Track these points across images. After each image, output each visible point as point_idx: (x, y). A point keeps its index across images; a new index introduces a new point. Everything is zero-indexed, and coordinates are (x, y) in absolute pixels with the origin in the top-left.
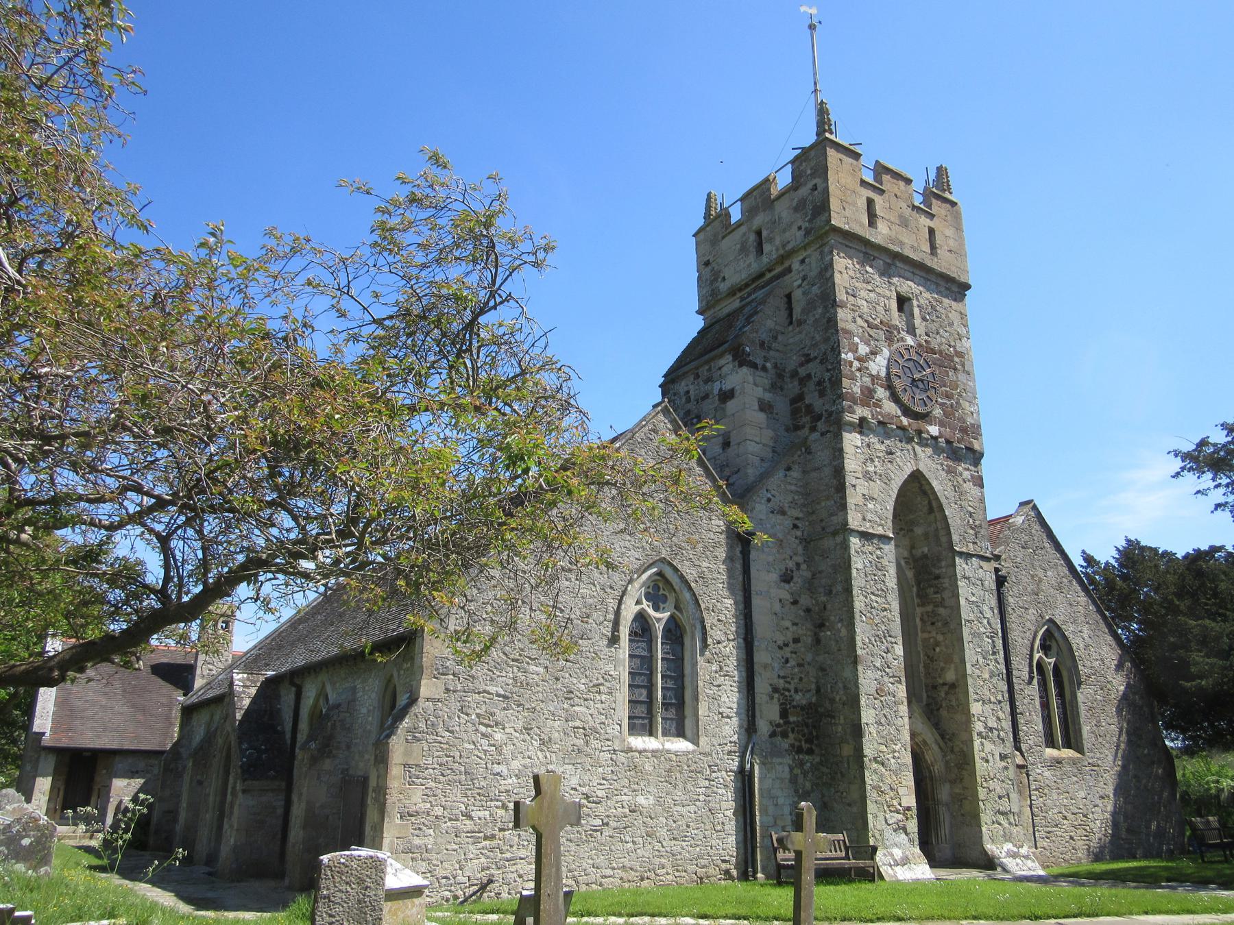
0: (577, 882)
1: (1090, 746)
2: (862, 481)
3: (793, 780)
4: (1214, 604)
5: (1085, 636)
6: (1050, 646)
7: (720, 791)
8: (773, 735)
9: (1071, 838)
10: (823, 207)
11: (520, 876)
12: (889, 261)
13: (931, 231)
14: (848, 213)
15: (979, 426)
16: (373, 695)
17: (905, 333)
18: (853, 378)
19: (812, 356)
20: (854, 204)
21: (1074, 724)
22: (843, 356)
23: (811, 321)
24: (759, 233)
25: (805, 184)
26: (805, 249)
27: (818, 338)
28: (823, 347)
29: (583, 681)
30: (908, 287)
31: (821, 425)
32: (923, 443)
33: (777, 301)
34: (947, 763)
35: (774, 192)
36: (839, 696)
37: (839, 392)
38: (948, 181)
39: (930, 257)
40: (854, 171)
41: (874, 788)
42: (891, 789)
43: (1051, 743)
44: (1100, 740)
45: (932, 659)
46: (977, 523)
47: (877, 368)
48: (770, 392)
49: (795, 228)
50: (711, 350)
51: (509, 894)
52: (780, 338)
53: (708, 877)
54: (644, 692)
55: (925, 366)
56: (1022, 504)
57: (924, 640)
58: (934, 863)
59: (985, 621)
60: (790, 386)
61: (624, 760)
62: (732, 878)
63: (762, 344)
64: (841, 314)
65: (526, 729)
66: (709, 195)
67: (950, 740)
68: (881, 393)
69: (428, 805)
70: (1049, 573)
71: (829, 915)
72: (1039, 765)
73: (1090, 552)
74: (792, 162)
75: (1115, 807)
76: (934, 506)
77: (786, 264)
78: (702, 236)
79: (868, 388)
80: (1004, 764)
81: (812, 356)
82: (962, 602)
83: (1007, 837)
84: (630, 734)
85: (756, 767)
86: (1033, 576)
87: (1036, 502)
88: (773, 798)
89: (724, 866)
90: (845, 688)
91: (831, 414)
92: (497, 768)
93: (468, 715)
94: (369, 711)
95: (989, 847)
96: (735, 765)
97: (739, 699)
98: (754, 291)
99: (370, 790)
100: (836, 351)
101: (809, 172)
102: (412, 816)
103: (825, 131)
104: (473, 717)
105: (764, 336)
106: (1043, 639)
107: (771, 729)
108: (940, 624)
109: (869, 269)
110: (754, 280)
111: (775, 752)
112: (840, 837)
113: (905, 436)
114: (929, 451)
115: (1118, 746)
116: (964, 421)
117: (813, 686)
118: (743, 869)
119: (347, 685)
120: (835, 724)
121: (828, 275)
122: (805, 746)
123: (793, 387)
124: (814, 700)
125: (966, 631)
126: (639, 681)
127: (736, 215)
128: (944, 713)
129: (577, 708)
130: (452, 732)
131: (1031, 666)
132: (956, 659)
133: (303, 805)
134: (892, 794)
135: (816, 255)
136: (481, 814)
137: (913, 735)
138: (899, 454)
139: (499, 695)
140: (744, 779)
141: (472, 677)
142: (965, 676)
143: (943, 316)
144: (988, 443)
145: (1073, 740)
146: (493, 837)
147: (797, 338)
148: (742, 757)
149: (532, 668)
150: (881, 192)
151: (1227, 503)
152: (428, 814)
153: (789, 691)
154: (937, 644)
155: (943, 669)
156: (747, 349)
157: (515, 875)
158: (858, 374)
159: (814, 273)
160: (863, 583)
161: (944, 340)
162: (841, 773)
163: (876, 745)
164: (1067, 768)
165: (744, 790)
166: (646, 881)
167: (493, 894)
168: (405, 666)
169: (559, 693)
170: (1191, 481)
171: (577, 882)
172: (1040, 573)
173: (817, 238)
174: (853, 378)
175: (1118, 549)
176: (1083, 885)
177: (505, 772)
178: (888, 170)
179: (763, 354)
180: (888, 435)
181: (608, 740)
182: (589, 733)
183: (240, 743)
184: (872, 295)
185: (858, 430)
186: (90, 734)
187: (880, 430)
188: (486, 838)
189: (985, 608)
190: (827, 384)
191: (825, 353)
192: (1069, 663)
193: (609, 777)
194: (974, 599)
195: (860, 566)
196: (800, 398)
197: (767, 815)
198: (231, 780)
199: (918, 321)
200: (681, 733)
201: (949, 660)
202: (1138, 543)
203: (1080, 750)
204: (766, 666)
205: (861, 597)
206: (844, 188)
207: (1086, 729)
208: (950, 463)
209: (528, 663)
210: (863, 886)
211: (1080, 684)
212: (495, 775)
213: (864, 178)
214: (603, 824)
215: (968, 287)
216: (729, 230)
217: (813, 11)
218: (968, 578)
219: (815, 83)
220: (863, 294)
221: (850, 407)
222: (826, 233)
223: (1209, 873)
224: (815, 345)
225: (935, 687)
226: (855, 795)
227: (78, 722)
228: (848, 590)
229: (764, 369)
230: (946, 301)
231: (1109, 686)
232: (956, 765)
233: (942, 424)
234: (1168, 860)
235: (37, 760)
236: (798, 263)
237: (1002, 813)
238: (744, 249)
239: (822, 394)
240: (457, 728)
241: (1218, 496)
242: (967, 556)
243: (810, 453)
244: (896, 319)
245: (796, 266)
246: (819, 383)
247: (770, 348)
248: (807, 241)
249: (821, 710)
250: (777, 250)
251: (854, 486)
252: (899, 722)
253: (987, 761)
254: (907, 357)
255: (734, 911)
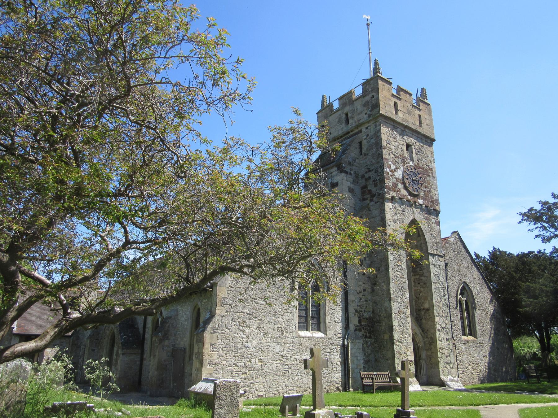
0: (279, 392)
1: (479, 335)
2: (393, 223)
3: (364, 349)
4: (531, 276)
5: (478, 289)
6: (464, 293)
7: (335, 354)
8: (355, 330)
9: (472, 373)
10: (376, 105)
11: (257, 390)
12: (403, 129)
13: (420, 116)
14: (387, 108)
15: (438, 200)
16: (188, 313)
17: (409, 160)
18: (389, 179)
19: (371, 169)
20: (389, 104)
21: (473, 326)
22: (385, 170)
23: (370, 154)
24: (347, 115)
25: (368, 95)
26: (368, 123)
27: (374, 161)
28: (376, 166)
29: (280, 307)
30: (410, 140)
31: (375, 199)
32: (416, 207)
33: (355, 145)
34: (424, 342)
35: (354, 97)
36: (383, 314)
37: (383, 185)
38: (426, 95)
39: (419, 127)
40: (389, 90)
41: (398, 352)
42: (404, 353)
43: (464, 334)
44: (484, 332)
45: (418, 298)
46: (438, 241)
47: (399, 175)
48: (353, 184)
49: (363, 114)
50: (327, 165)
51: (252, 397)
52: (357, 160)
53: (330, 390)
54: (304, 312)
55: (417, 174)
56: (453, 233)
57: (415, 290)
58: (421, 384)
59: (441, 283)
60: (361, 181)
61: (297, 341)
62: (340, 390)
63: (350, 163)
64: (385, 152)
65: (258, 328)
66: (323, 96)
67: (426, 333)
68: (400, 186)
69: (220, 360)
70: (464, 262)
71: (392, 405)
72: (460, 343)
73: (477, 252)
74: (363, 84)
75: (489, 360)
76: (420, 233)
77: (359, 129)
78: (320, 114)
79: (395, 184)
80: (448, 343)
81: (371, 169)
82: (432, 274)
83: (449, 373)
84: (299, 330)
85: (350, 344)
86: (457, 263)
87: (459, 232)
88: (356, 357)
89: (337, 385)
90: (385, 310)
91: (379, 194)
92: (247, 345)
93: (235, 322)
94: (185, 320)
95: (442, 377)
96: (340, 343)
97: (342, 315)
98: (345, 139)
99: (194, 354)
100: (382, 167)
101: (370, 90)
102: (213, 365)
103: (377, 72)
104: (237, 323)
105: (351, 160)
106: (461, 290)
107: (355, 328)
108: (422, 284)
109: (395, 132)
110: (344, 135)
111: (357, 338)
112: (387, 373)
113: (410, 204)
114: (419, 210)
115: (490, 335)
116: (433, 198)
117: (371, 310)
118: (344, 386)
119: (173, 308)
120: (381, 326)
121: (379, 135)
122: (368, 335)
123: (362, 182)
124: (371, 315)
125: (433, 287)
126: (302, 307)
127: (336, 105)
128: (423, 321)
129: (278, 319)
130: (229, 329)
131: (456, 301)
132: (429, 298)
133: (156, 360)
134: (405, 355)
135: (373, 126)
136: (241, 364)
137: (412, 330)
138: (407, 211)
139: (247, 314)
140: (344, 348)
141: (237, 306)
142: (433, 306)
143: (424, 153)
144: (443, 207)
145: (473, 333)
146: (246, 373)
147: (364, 161)
148: (344, 340)
149: (260, 302)
150: (400, 99)
151: (540, 235)
152: (220, 364)
153: (362, 312)
154: (421, 292)
155: (423, 303)
156: (344, 165)
157: (255, 389)
158: (391, 178)
159: (372, 133)
160: (393, 266)
161: (424, 163)
162: (384, 346)
163: (398, 335)
164: (471, 344)
165: (345, 354)
166: (306, 392)
167: (246, 398)
168: (204, 301)
169: (271, 313)
170: (527, 225)
171: (279, 392)
172: (460, 262)
173: (373, 119)
174: (389, 179)
175: (489, 252)
176: (483, 392)
177: (250, 346)
178: (403, 90)
179: (350, 167)
180: (402, 204)
181: (291, 332)
182: (283, 330)
183: (120, 333)
184: (396, 143)
185: (391, 201)
186: (35, 328)
187: (399, 201)
188: (243, 374)
189: (441, 277)
190: (378, 181)
191: (377, 168)
192: (471, 300)
193: (291, 348)
194: (436, 273)
195: (392, 259)
196: (365, 187)
197: (354, 364)
198: (115, 349)
199: (414, 155)
200: (319, 330)
201: (426, 299)
202: (499, 249)
203: (476, 337)
204: (352, 301)
205: (392, 272)
206: (385, 98)
207: (478, 328)
208: (427, 216)
209: (259, 300)
210: (388, 394)
211: (476, 309)
212: (246, 347)
213: (393, 93)
214: (289, 368)
215: (434, 140)
216: (333, 112)
217: (368, 17)
218: (434, 264)
219: (369, 49)
220: (393, 143)
221: (388, 191)
222: (378, 117)
223: (534, 388)
224: (372, 165)
225: (419, 310)
226: (389, 355)
227: (28, 323)
228: (387, 269)
229: (351, 174)
230: (425, 146)
231: (487, 310)
232: (429, 343)
233: (424, 199)
234: (515, 382)
235: (11, 340)
236: (365, 129)
237: (447, 363)
238: (340, 121)
239: (376, 185)
240: (231, 328)
241: (536, 232)
242: (434, 255)
243: (370, 211)
244: (406, 154)
245: (364, 130)
246: (374, 181)
247: (353, 165)
248: (369, 119)
249: (375, 320)
250: (355, 122)
251: (389, 225)
252: (407, 325)
253: (442, 341)
254: (410, 170)
255: (353, 403)
